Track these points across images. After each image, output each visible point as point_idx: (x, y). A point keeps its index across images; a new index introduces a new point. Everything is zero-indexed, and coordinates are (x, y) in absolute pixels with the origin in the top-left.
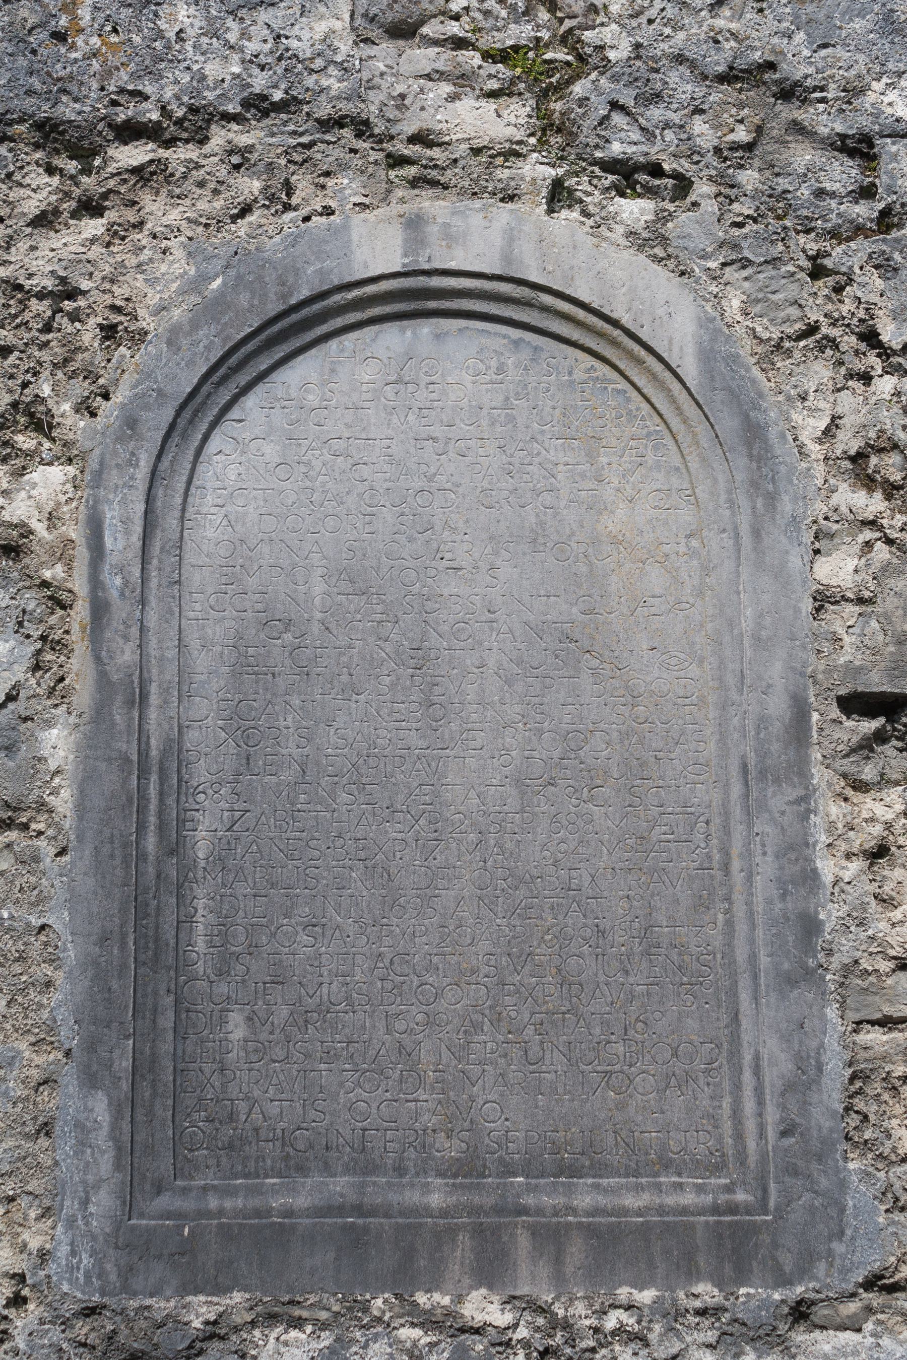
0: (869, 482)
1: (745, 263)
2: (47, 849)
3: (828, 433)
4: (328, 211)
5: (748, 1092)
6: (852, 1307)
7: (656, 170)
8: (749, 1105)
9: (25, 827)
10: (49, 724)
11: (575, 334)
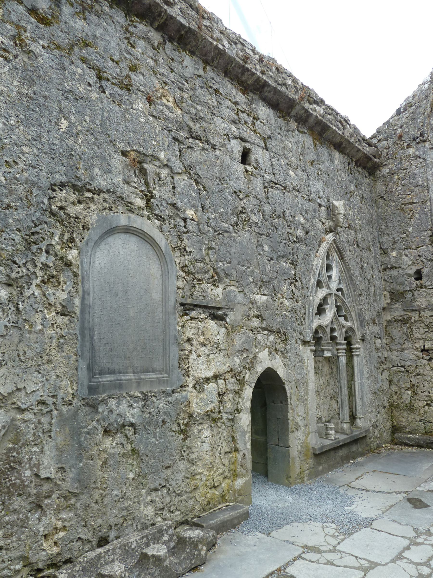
0: (183, 271)
1: (171, 235)
2: (75, 320)
3: (179, 263)
4: (117, 213)
5: (168, 360)
6: (179, 390)
7: (161, 217)
8: (168, 362)
9: (71, 316)
10: (75, 298)
11: (147, 240)
